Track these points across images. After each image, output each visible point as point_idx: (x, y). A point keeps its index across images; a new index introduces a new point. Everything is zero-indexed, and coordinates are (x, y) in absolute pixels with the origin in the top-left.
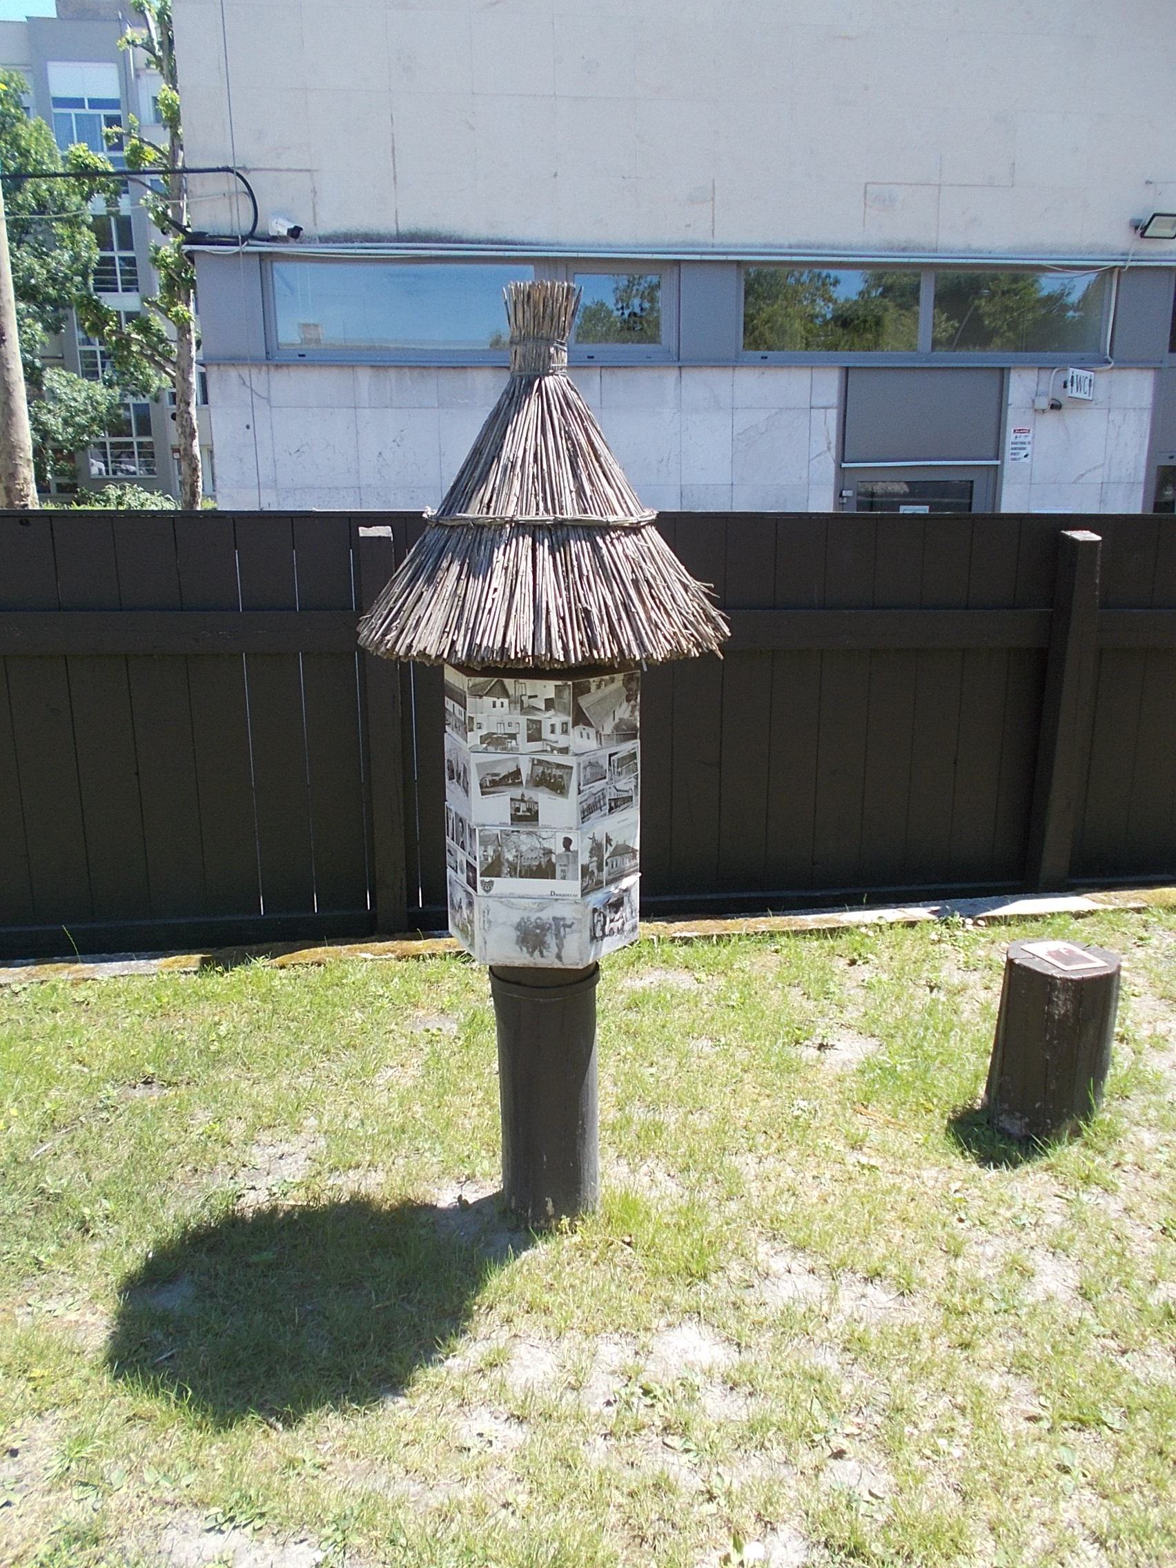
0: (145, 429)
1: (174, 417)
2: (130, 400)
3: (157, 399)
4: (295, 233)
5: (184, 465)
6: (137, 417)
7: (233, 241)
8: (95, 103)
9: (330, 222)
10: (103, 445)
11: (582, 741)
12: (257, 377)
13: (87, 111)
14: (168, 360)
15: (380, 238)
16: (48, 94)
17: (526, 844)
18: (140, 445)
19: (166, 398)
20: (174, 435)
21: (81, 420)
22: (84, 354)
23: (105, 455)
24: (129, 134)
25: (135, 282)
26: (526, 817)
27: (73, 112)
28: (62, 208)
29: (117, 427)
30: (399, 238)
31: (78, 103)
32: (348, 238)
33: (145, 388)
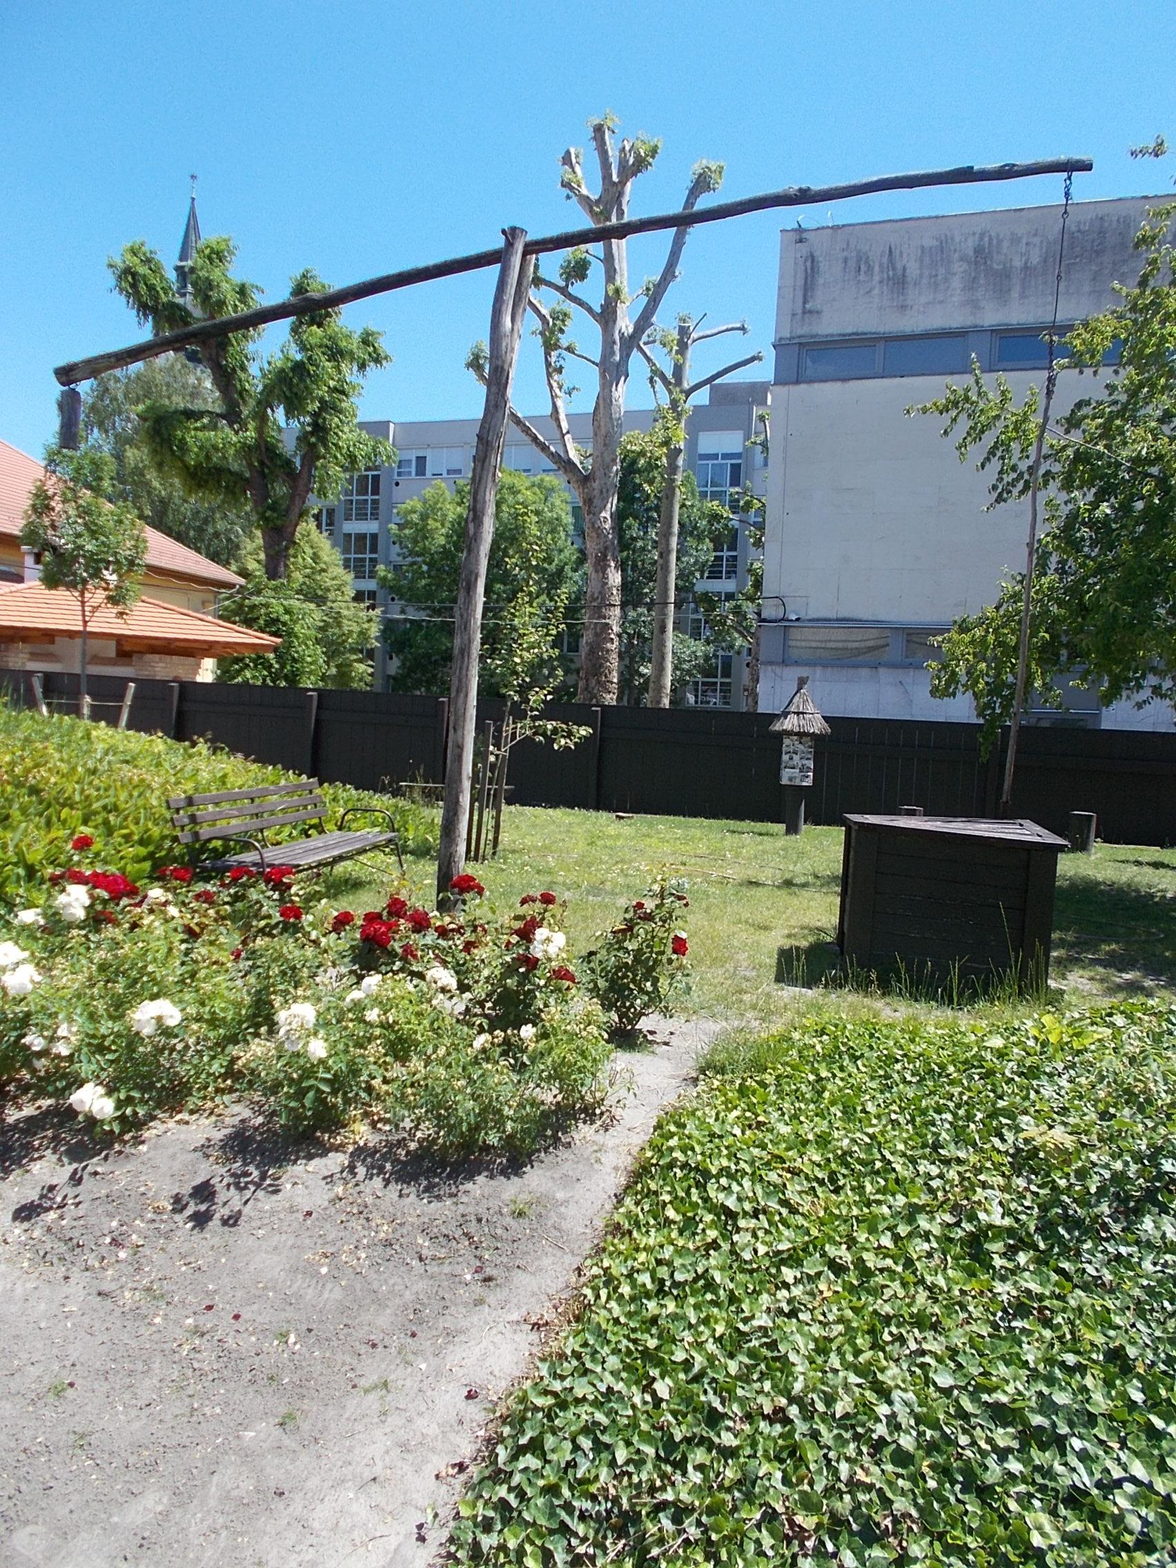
0: (726, 673)
1: (748, 665)
2: (721, 653)
3: (739, 653)
4: (798, 620)
5: (750, 699)
6: (723, 663)
7: (775, 621)
8: (726, 456)
9: (812, 614)
10: (696, 683)
11: (801, 747)
12: (778, 670)
13: (720, 461)
14: (749, 632)
15: (830, 620)
16: (696, 449)
17: (791, 763)
18: (722, 684)
19: (745, 652)
20: (746, 679)
21: (686, 666)
22: (694, 621)
23: (696, 690)
24: (745, 493)
25: (735, 572)
26: (791, 759)
27: (710, 462)
28: (695, 528)
29: (709, 671)
30: (837, 620)
31: (715, 456)
32: (818, 620)
33: (731, 647)
